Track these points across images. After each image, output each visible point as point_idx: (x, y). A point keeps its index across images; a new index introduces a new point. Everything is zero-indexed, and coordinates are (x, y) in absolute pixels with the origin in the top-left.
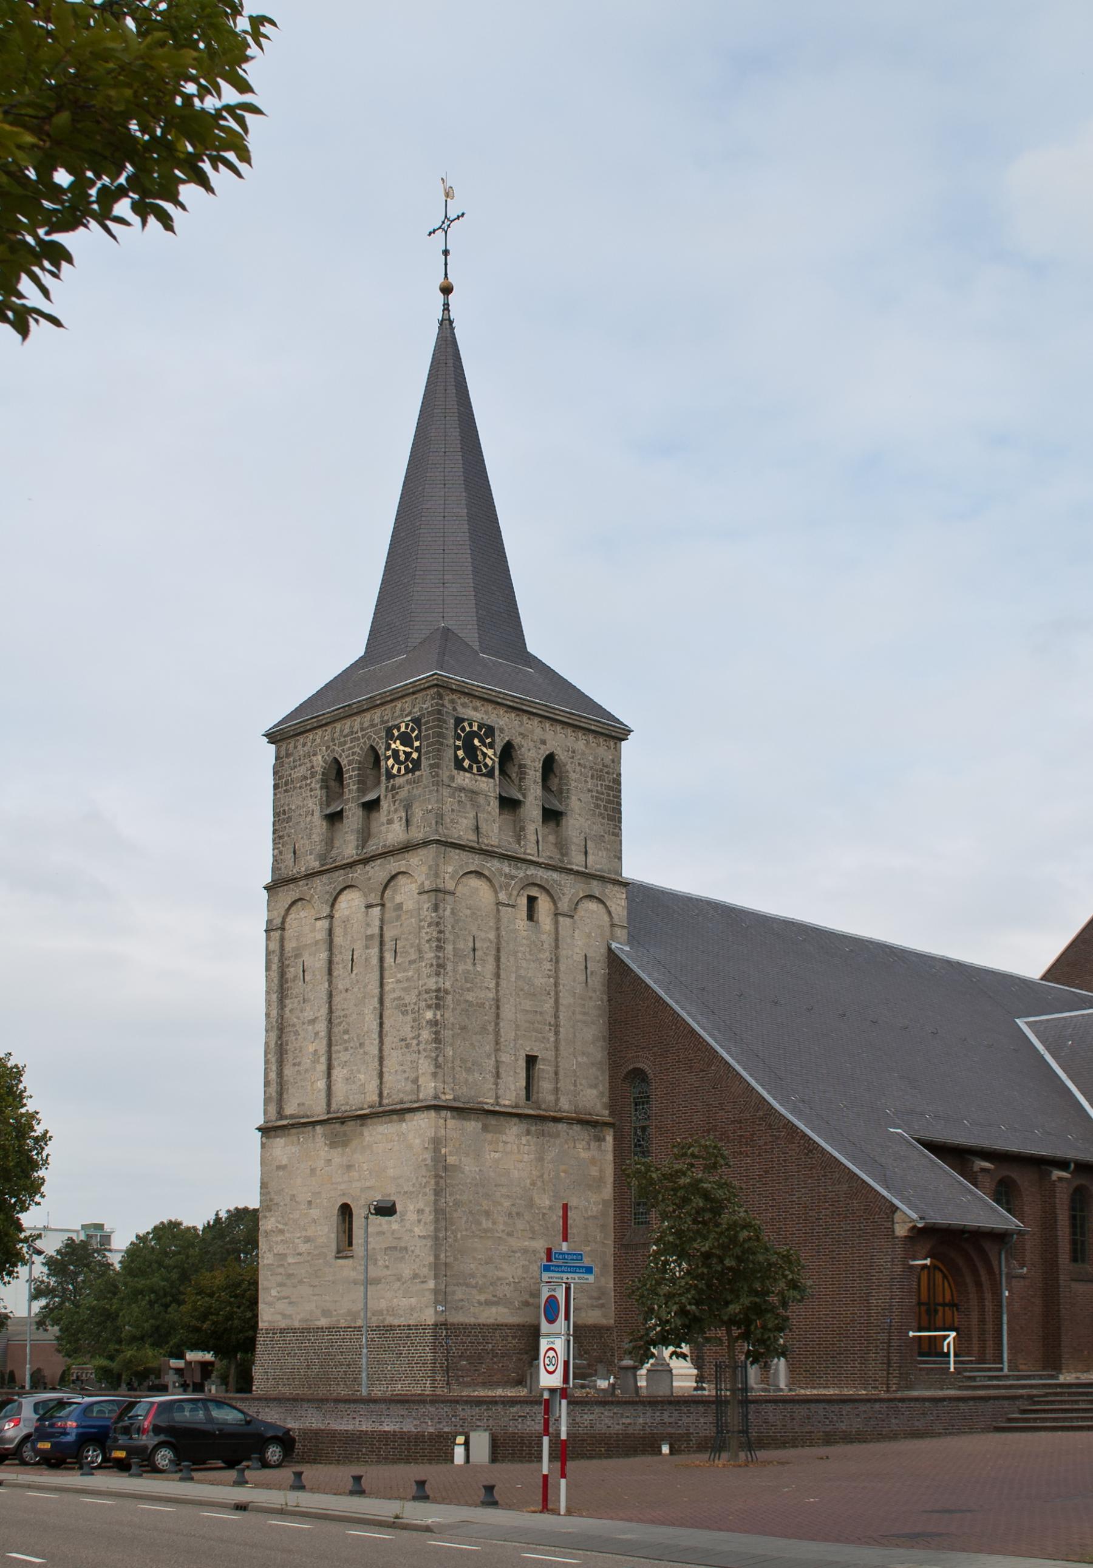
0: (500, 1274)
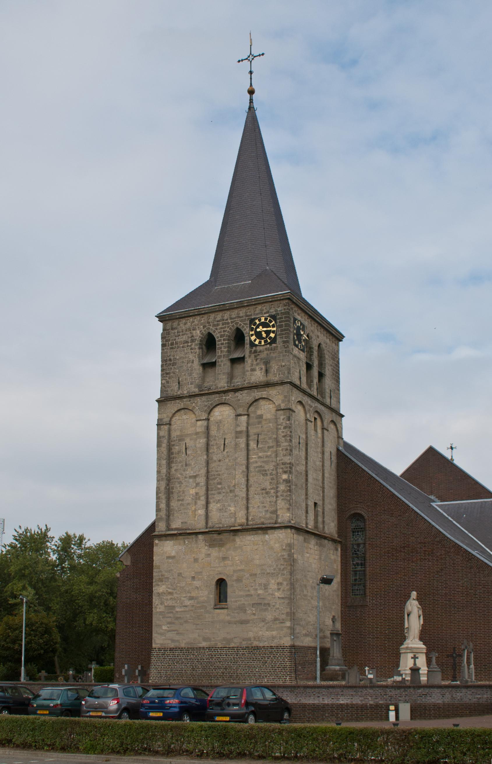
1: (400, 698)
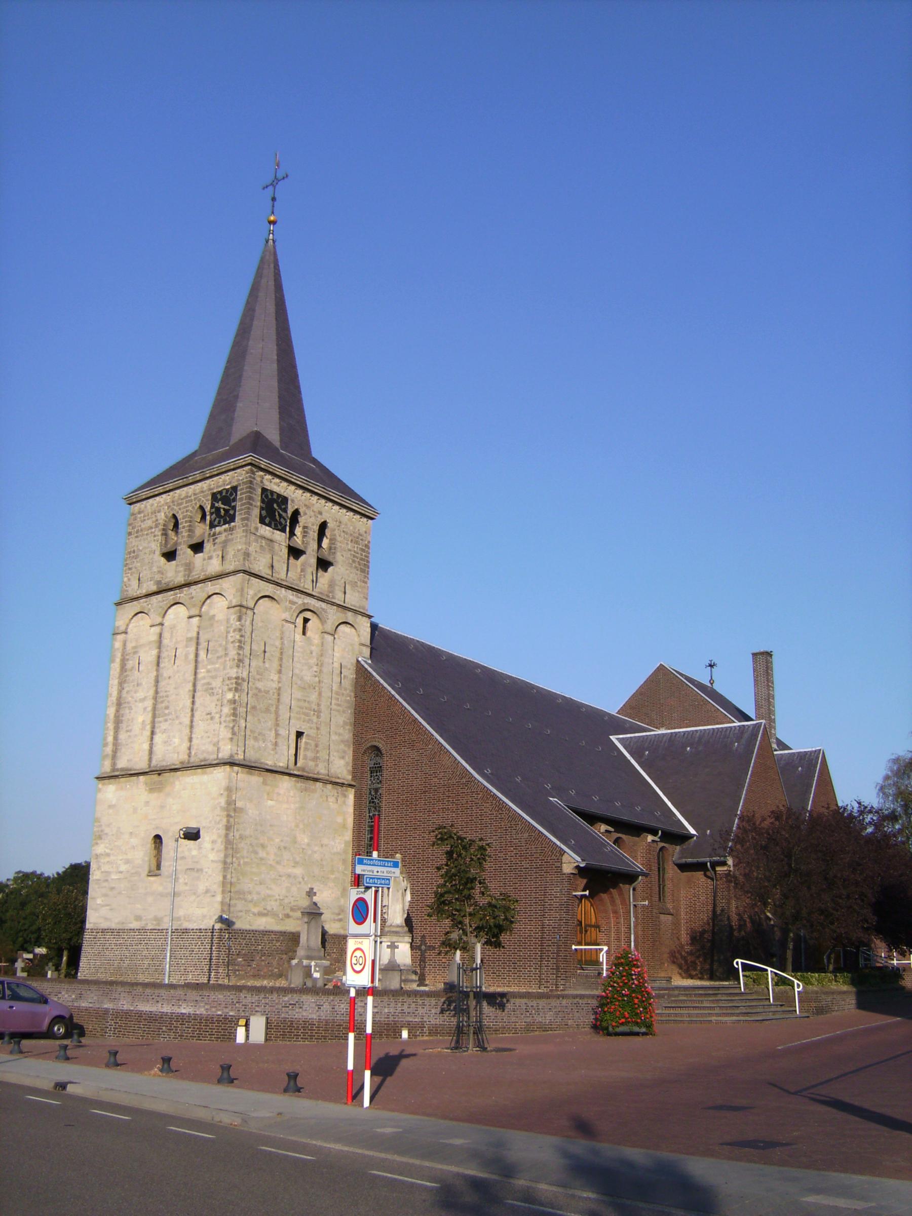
0: (268, 892)
1: (257, 1009)
